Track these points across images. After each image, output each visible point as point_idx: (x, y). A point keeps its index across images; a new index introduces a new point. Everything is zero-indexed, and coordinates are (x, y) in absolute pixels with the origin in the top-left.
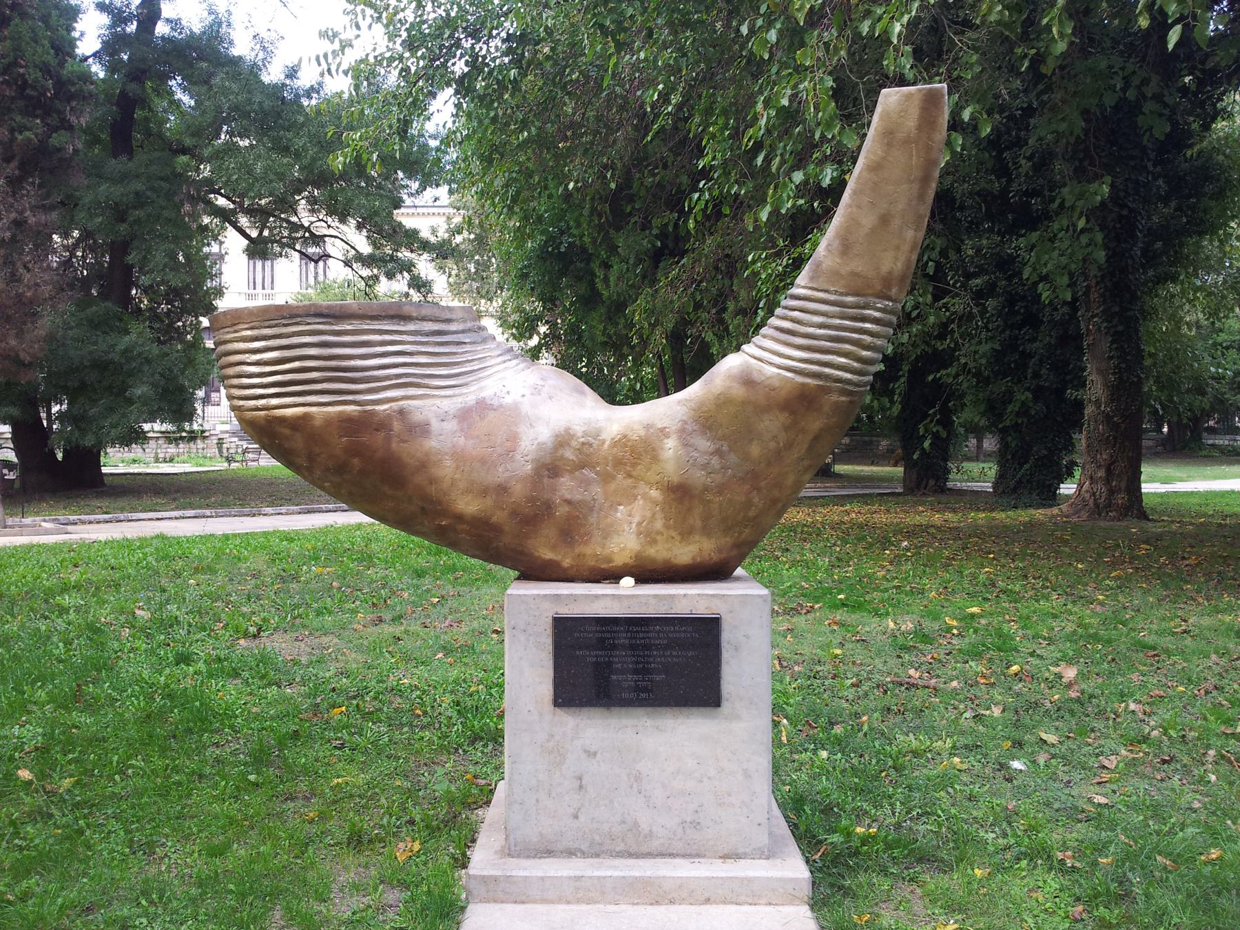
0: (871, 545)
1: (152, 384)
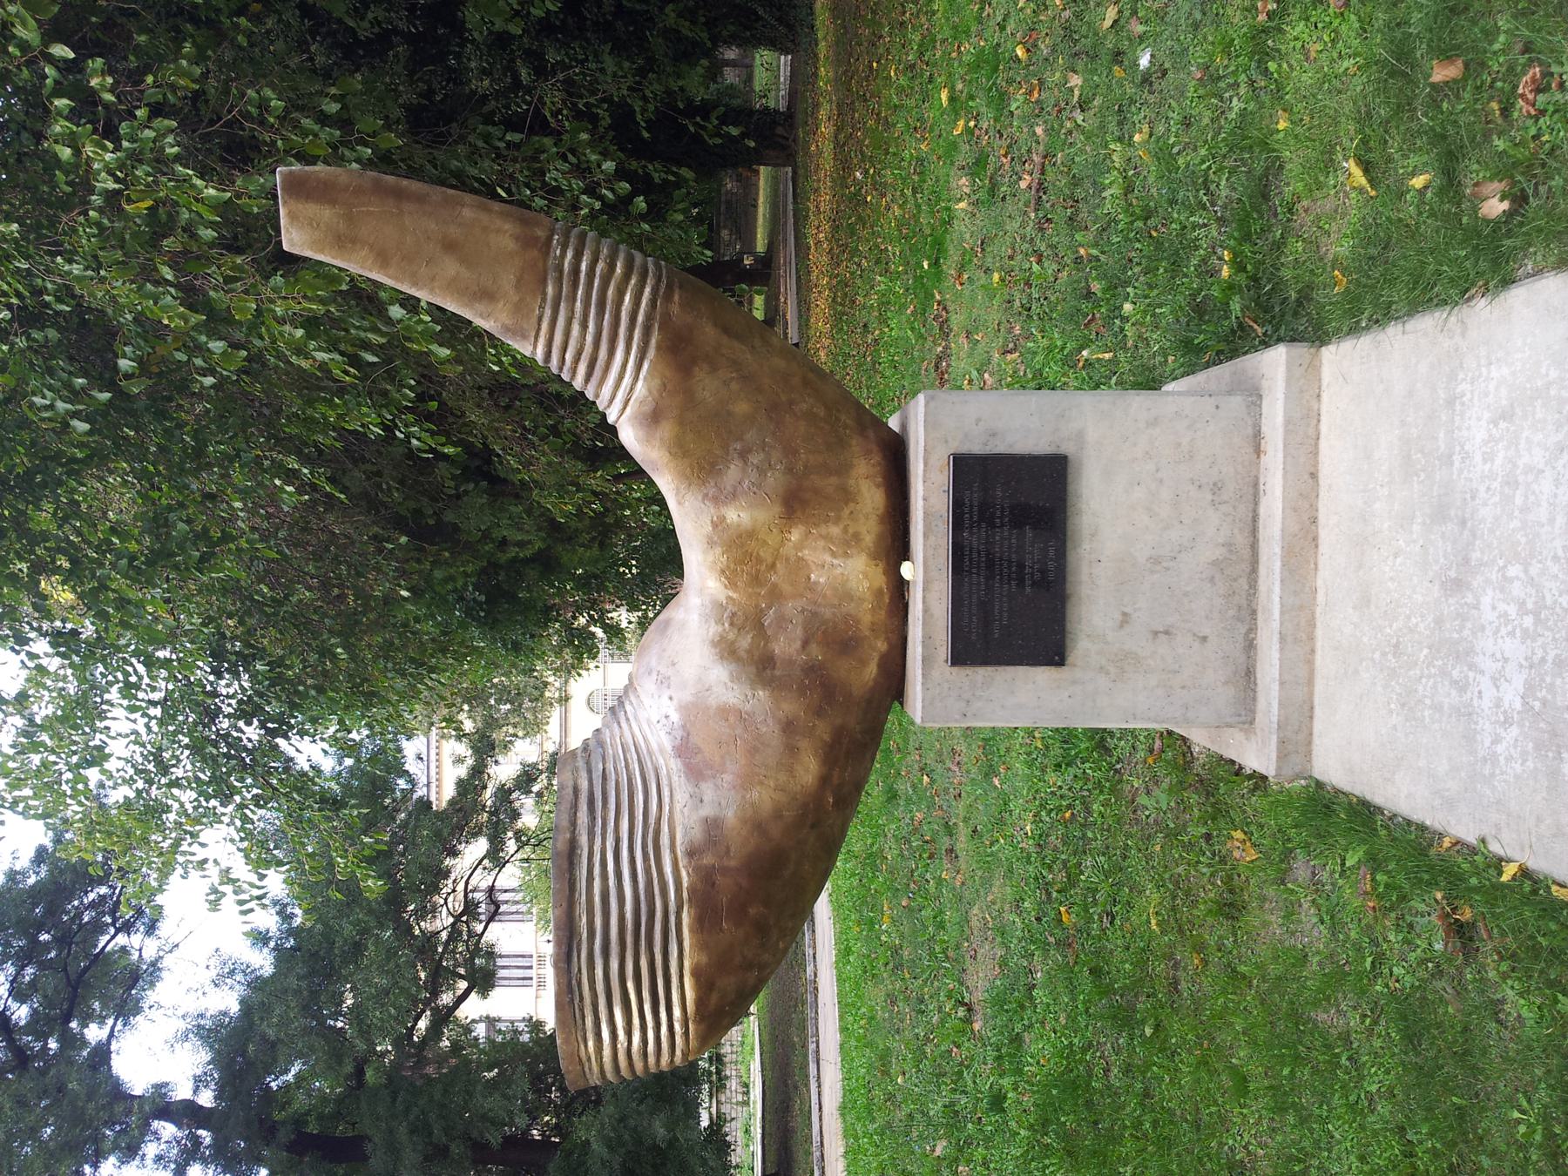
0: (860, 218)
1: (651, 1114)
